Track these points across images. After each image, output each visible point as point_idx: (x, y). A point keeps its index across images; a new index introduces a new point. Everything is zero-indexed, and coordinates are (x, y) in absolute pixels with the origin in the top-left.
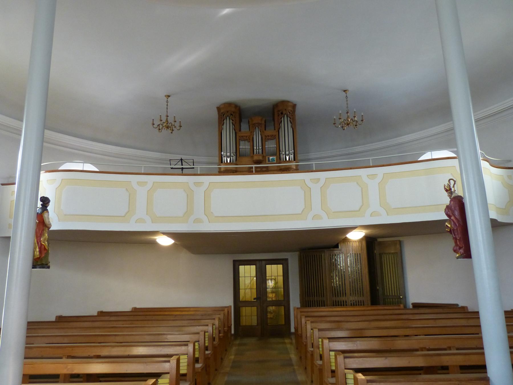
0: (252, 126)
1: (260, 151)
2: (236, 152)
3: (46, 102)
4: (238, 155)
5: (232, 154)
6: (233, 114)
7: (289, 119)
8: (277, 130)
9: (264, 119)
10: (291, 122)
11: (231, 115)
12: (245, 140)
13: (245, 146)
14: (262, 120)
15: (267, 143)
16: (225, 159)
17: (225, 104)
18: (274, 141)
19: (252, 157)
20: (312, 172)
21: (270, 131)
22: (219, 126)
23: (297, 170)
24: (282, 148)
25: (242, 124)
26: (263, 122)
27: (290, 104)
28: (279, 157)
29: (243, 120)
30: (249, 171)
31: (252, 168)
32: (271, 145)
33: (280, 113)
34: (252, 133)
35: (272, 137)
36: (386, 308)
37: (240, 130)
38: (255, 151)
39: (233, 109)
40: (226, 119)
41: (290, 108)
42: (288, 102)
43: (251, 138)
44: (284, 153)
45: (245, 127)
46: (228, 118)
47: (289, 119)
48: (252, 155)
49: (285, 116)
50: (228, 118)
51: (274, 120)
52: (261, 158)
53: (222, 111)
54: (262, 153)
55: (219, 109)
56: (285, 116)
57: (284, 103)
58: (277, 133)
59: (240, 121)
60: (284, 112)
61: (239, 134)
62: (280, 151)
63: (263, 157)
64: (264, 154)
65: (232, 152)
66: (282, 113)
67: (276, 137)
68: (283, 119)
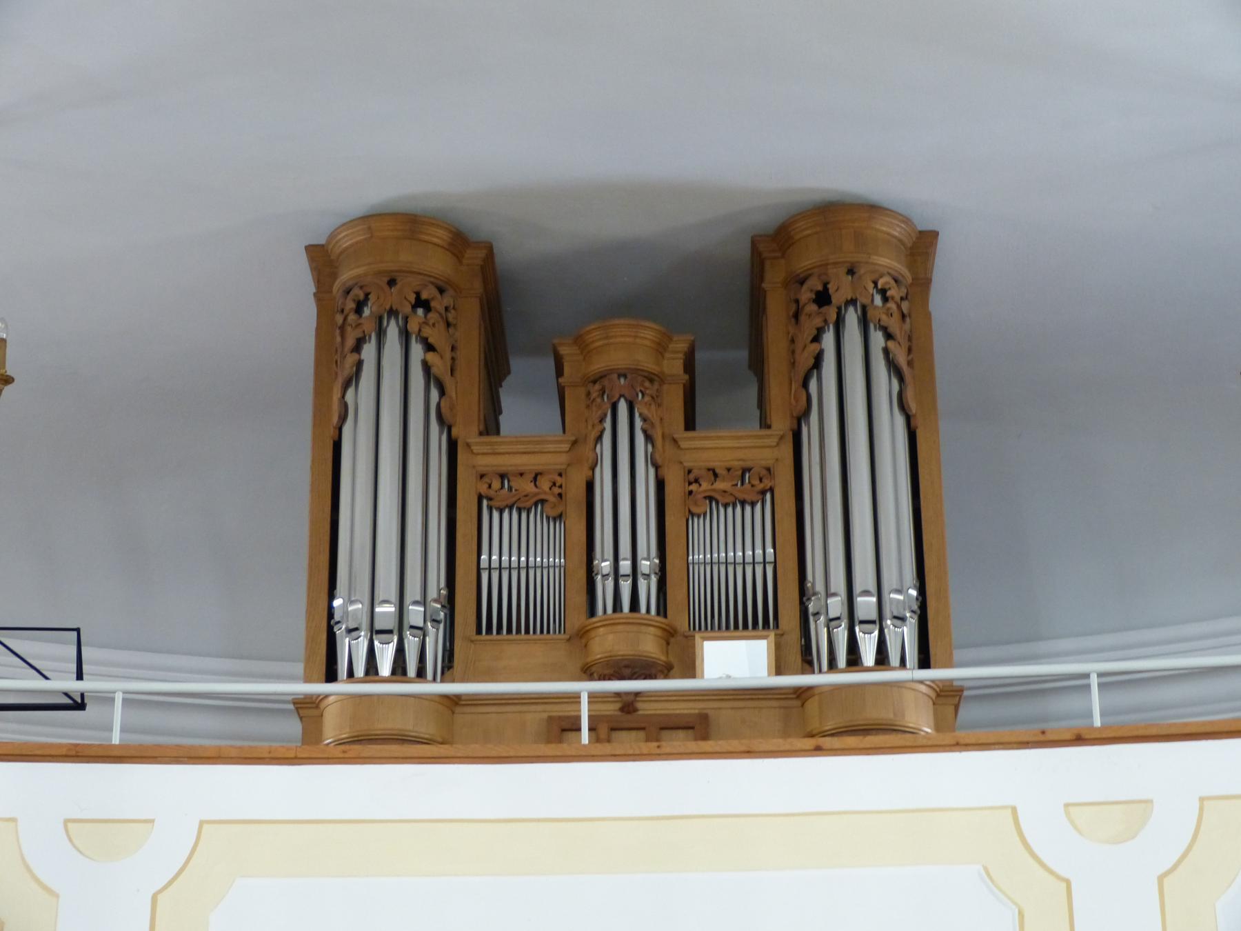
0: (590, 396)
1: (648, 589)
2: (450, 602)
3: (66, 756)
4: (472, 618)
5: (415, 614)
6: (449, 312)
7: (877, 339)
8: (781, 424)
9: (680, 345)
10: (893, 367)
11: (420, 303)
12: (520, 506)
13: (522, 553)
14: (660, 349)
15: (699, 527)
16: (352, 648)
17: (371, 220)
18: (759, 515)
19: (582, 636)
20: (1079, 740)
21: (727, 443)
22: (321, 391)
23: (958, 721)
24: (823, 564)
25: (508, 400)
26: (674, 366)
27: (883, 226)
28: (794, 637)
29: (516, 363)
30: (555, 735)
31: (574, 698)
32: (731, 546)
33: (806, 295)
34: (580, 445)
35: (748, 487)
36: (266, 744)
37: (491, 427)
38: (604, 589)
39: (439, 264)
40: (381, 333)
41: (888, 262)
42: (872, 209)
43: (576, 490)
44: (836, 606)
45: (527, 415)
46: (393, 331)
47: (877, 339)
48: (577, 618)
49: (852, 318)
50: (393, 331)
51: (758, 364)
52: (649, 646)
53: (346, 275)
54: (662, 609)
55: (322, 260)
56: (852, 318)
57: (837, 217)
58: (787, 450)
59: (495, 370)
60: (841, 290)
61: (481, 456)
62: (803, 592)
63: (669, 635)
64: (678, 617)
65: (413, 591)
66: (823, 298)
67: (779, 489)
68: (828, 339)
